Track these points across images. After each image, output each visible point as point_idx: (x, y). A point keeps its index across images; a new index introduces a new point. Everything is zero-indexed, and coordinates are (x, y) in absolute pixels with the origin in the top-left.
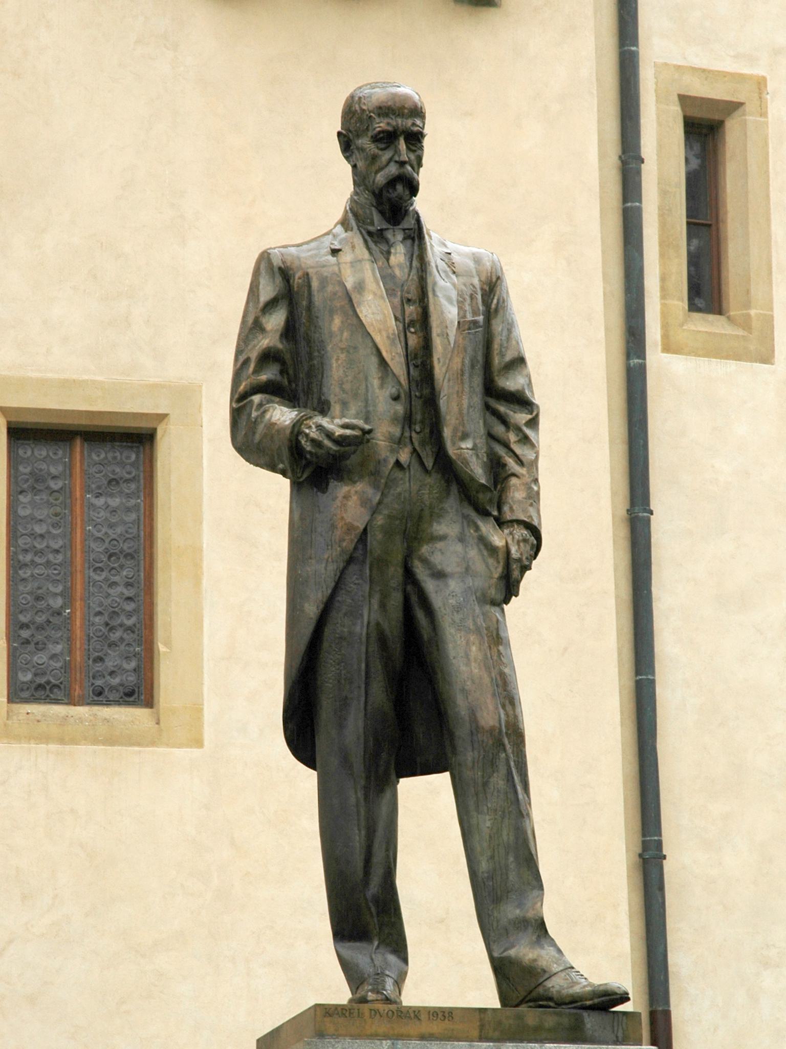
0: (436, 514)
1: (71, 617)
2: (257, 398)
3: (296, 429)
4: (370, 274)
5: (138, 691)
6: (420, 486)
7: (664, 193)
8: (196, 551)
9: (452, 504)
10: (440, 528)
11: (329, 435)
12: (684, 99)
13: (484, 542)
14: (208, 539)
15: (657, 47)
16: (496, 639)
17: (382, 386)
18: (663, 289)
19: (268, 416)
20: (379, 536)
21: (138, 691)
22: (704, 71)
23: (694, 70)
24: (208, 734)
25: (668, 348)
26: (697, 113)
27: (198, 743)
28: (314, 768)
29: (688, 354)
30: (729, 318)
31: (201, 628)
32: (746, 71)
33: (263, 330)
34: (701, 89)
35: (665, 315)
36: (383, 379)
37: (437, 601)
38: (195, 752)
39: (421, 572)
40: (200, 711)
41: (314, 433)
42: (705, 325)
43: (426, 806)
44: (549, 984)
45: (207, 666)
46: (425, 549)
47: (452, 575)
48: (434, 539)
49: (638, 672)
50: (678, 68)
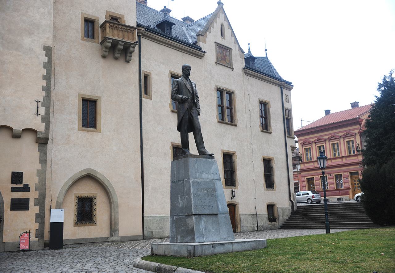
0: (193, 107)
1: (88, 119)
2: (176, 94)
5: (83, 126)
7: (143, 83)
9: (194, 106)
10: (193, 108)
11: (186, 98)
13: (197, 110)
15: (142, 69)
16: (198, 119)
21: (83, 126)
34: (146, 73)
36: (189, 93)
37: (193, 115)
38: (101, 133)
39: (191, 113)
40: (101, 129)
42: (146, 95)
43: (191, 135)
46: (192, 110)
48: (192, 109)
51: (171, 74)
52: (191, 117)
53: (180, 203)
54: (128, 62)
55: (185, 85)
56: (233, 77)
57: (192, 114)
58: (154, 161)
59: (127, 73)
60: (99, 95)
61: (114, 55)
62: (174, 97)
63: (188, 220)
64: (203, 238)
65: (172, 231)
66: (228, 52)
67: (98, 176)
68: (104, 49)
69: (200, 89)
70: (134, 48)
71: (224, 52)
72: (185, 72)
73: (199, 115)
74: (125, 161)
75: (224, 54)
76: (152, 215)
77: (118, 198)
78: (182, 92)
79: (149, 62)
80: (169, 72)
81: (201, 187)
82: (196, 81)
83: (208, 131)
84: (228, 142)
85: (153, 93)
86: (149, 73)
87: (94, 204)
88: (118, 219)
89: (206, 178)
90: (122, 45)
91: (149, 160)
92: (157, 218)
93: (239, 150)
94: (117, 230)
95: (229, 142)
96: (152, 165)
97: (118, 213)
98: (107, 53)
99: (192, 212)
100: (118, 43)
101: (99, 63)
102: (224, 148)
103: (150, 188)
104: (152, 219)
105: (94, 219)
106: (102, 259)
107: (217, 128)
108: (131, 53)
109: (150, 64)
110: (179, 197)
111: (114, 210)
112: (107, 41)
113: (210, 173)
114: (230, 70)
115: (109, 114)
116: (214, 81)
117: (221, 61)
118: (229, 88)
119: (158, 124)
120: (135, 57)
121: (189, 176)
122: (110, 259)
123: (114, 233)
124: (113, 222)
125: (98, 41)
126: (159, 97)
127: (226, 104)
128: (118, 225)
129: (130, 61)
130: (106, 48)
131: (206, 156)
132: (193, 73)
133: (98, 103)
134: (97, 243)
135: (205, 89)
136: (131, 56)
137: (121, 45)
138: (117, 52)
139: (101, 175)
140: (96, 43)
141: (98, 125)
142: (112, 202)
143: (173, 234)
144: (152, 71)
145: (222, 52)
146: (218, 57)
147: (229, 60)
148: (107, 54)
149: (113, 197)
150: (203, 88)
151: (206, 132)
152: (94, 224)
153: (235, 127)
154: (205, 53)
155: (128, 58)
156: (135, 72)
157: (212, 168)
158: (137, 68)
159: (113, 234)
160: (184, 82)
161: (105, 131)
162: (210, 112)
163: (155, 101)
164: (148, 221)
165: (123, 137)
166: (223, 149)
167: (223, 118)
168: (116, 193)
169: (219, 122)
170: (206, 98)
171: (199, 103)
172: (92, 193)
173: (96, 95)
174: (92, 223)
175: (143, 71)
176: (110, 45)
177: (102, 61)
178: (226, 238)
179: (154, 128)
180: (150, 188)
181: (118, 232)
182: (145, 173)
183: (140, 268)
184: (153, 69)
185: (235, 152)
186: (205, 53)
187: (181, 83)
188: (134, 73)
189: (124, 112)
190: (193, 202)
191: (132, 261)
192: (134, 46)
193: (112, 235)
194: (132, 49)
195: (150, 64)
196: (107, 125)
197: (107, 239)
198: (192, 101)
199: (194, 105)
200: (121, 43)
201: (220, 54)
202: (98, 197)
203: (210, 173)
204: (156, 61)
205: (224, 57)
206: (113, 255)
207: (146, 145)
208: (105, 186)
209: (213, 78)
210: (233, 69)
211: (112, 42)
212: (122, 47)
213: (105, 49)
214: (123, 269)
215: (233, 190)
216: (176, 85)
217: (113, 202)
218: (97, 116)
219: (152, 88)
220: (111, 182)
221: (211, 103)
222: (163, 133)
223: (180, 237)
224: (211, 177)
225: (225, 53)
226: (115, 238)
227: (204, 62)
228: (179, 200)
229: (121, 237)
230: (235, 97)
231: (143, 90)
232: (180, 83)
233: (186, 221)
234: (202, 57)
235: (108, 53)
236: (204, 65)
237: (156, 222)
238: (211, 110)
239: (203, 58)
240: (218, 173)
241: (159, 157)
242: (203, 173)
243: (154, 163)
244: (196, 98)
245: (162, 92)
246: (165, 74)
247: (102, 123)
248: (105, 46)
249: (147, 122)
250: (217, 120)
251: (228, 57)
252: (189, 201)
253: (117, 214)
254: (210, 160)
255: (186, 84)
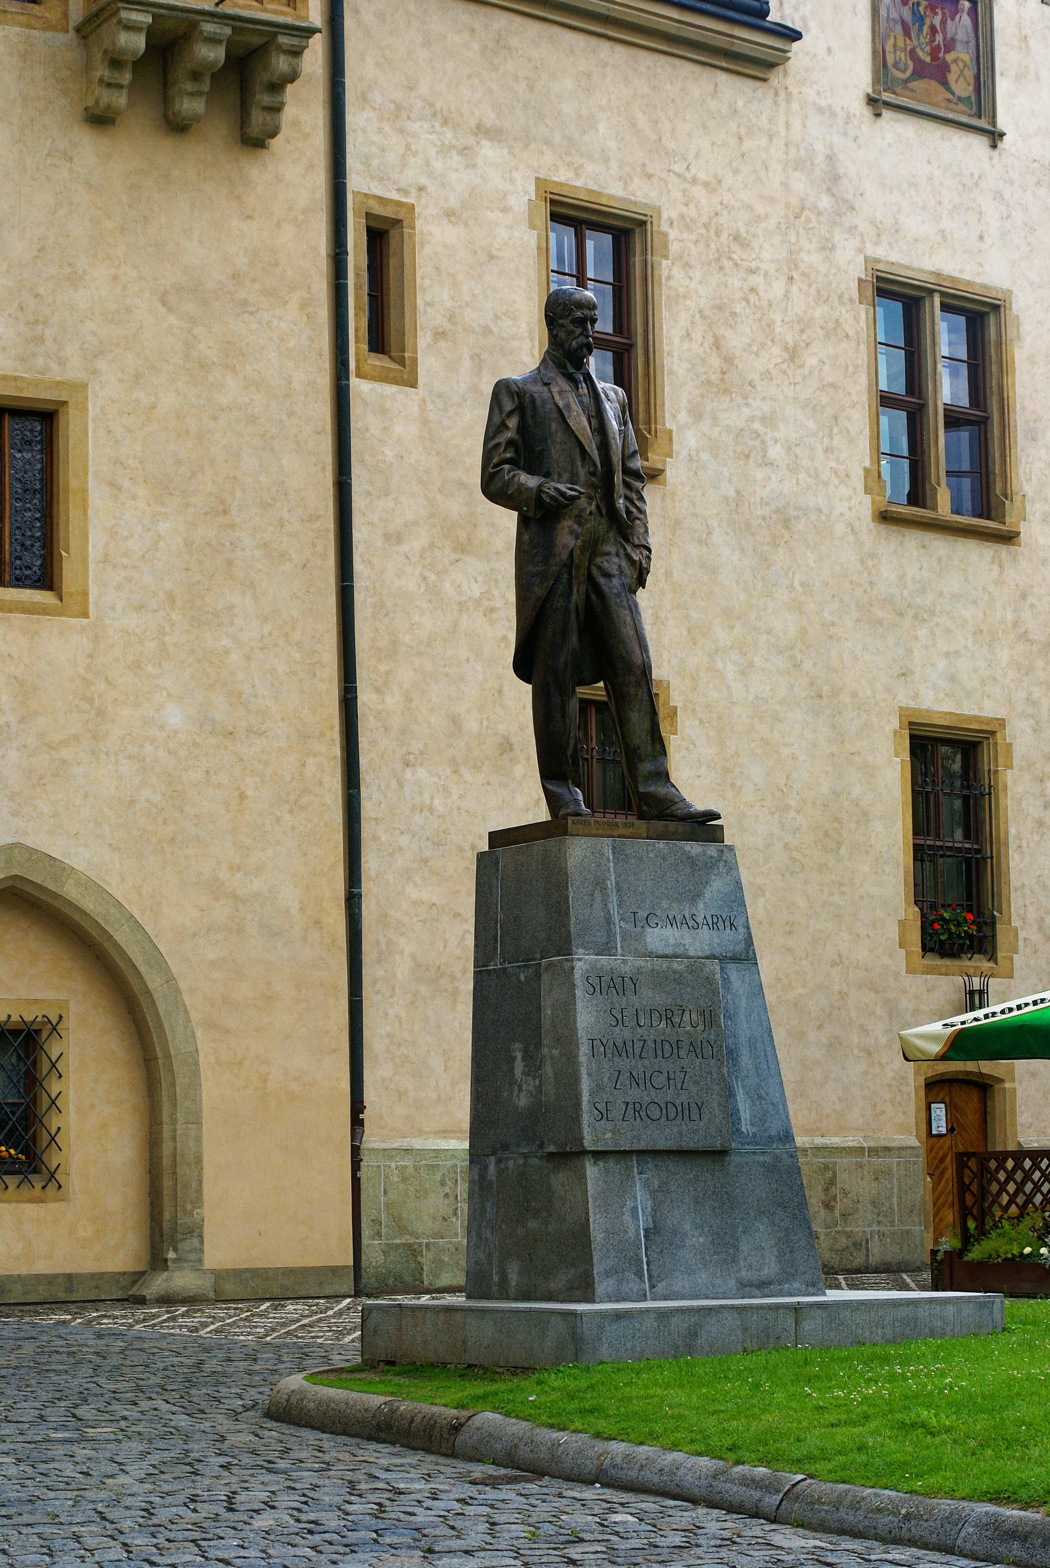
0: (605, 541)
2: (507, 467)
3: (540, 489)
4: (572, 400)
6: (602, 525)
7: (357, 275)
8: (85, 491)
12: (368, 215)
13: (628, 557)
14: (91, 484)
15: (356, 182)
16: (634, 610)
17: (582, 466)
18: (356, 336)
19: (516, 479)
20: (579, 552)
22: (380, 198)
23: (375, 197)
24: (92, 608)
25: (358, 376)
26: (374, 225)
27: (85, 615)
28: (529, 682)
29: (370, 379)
30: (390, 357)
31: (87, 541)
32: (404, 200)
33: (507, 428)
34: (378, 210)
35: (357, 354)
38: (84, 621)
39: (595, 572)
41: (553, 493)
44: (674, 808)
45: (91, 567)
46: (598, 560)
47: (614, 576)
49: (343, 581)
50: (366, 195)
51: (552, 201)
52: (593, 597)
53: (520, 1089)
54: (254, 140)
55: (555, 415)
56: (999, 196)
57: (602, 581)
58: (426, 796)
59: (249, 217)
60: (74, 371)
61: (166, 100)
62: (497, 485)
63: (560, 1180)
64: (641, 1277)
65: (479, 1236)
66: (966, 20)
67: (71, 891)
68: (101, 71)
69: (752, 298)
70: (297, 53)
71: (937, 21)
72: (562, 335)
73: (642, 583)
74: (242, 796)
75: (933, 30)
76: (418, 1143)
77: (199, 1034)
78: (541, 452)
79: (401, 131)
80: (537, 189)
81: (635, 1000)
82: (724, 237)
83: (802, 584)
84: (947, 654)
85: (423, 341)
86: (399, 204)
87: (45, 1066)
88: (199, 1160)
89: (669, 951)
90: (220, 42)
91: (394, 785)
92: (449, 1163)
93: (1029, 710)
94: (196, 1231)
95: (956, 652)
96: (418, 819)
97: (198, 1123)
98: (125, 91)
99: (581, 1139)
100: (194, 25)
101: (71, 160)
102: (917, 696)
103: (402, 969)
104: (416, 1168)
105: (54, 1159)
106: (102, 1381)
107: (870, 563)
108: (277, 87)
109: (408, 147)
110: (519, 1055)
111: (175, 1106)
112: (120, 22)
113: (691, 923)
114: (978, 144)
115: (134, 498)
116: (852, 229)
117: (914, 85)
118: (967, 277)
119: (455, 549)
120: (303, 111)
121: (568, 940)
122: (141, 1383)
123: (175, 1250)
124: (167, 1183)
125: (66, 15)
126: (467, 363)
127: (949, 389)
128: (198, 1202)
129: (273, 135)
130: (116, 63)
131: (672, 826)
132: (706, 184)
133: (70, 425)
134: (73, 1308)
135: (787, 296)
136: (277, 109)
137: (212, 40)
138: (189, 86)
139: (90, 885)
140: (48, 27)
141: (68, 570)
142: (159, 1054)
143: (482, 1256)
144: (421, 189)
145: (920, 19)
146: (890, 59)
147: (970, 74)
148: (121, 100)
149: (166, 1025)
150: (778, 288)
151: (791, 588)
152: (52, 1187)
153: (1003, 551)
154: (795, 36)
155: (258, 119)
156: (304, 212)
157: (707, 895)
158: (320, 180)
159: (171, 1255)
160: (557, 397)
161: (113, 608)
162: (826, 450)
163: (440, 396)
164: (386, 1177)
165: (226, 642)
166: (912, 704)
167: (918, 493)
168: (187, 999)
169: (885, 517)
170: (793, 354)
171: (641, 511)
172: (36, 1001)
173: (56, 373)
174: (38, 1186)
175: (356, 194)
176: (138, 42)
177: (88, 146)
178: (770, 1283)
179: (433, 577)
180: (402, 969)
181: (196, 1241)
182: (372, 873)
183: (298, 1424)
184: (423, 180)
185: (1002, 723)
186: (795, 36)
187: (538, 402)
188: (301, 217)
189: (234, 478)
190: (585, 1085)
191: (260, 1396)
192: (295, 41)
193: (157, 1261)
194: (281, 63)
195: (408, 147)
196: (125, 567)
197: (134, 1283)
198: (598, 507)
199: (610, 528)
200: (209, 28)
201: (907, 33)
202: (71, 1022)
203: (691, 923)
204: (445, 122)
205: (934, 53)
206: (161, 1365)
207: (378, 691)
208: (122, 964)
209: (852, 208)
210: (995, 137)
211: (150, 27)
212: (216, 55)
213: (107, 73)
214: (208, 1424)
215: (976, 980)
216: (510, 414)
217: (168, 1056)
218: (62, 507)
219: (420, 302)
220: (151, 934)
221: (833, 385)
222: (493, 610)
223: (520, 1272)
224: (699, 942)
225: (943, 23)
226: (181, 1280)
227: (783, 105)
228: (519, 1067)
229: (220, 1275)
230: (1011, 333)
231: (357, 322)
232: (533, 401)
233: (549, 1185)
234: (771, 66)
235: (130, 97)
236: (788, 125)
237: (443, 1184)
238: (831, 437)
239: (775, 78)
240: (739, 922)
241: (463, 770)
242: (653, 921)
243: (431, 810)
244: (627, 485)
245: (486, 331)
246: (505, 210)
247: (94, 553)
248: (106, 52)
249: (387, 537)
250: (873, 502)
251: (961, 57)
252: (569, 1081)
253: (192, 1133)
254: (693, 848)
255: (568, 406)
